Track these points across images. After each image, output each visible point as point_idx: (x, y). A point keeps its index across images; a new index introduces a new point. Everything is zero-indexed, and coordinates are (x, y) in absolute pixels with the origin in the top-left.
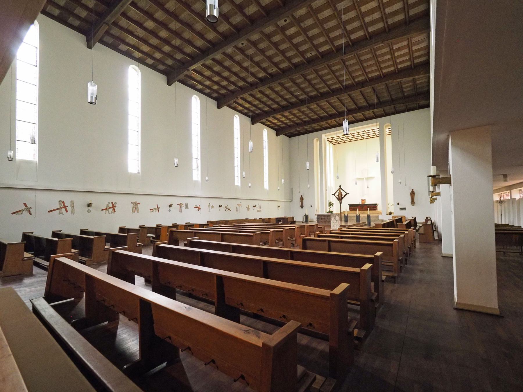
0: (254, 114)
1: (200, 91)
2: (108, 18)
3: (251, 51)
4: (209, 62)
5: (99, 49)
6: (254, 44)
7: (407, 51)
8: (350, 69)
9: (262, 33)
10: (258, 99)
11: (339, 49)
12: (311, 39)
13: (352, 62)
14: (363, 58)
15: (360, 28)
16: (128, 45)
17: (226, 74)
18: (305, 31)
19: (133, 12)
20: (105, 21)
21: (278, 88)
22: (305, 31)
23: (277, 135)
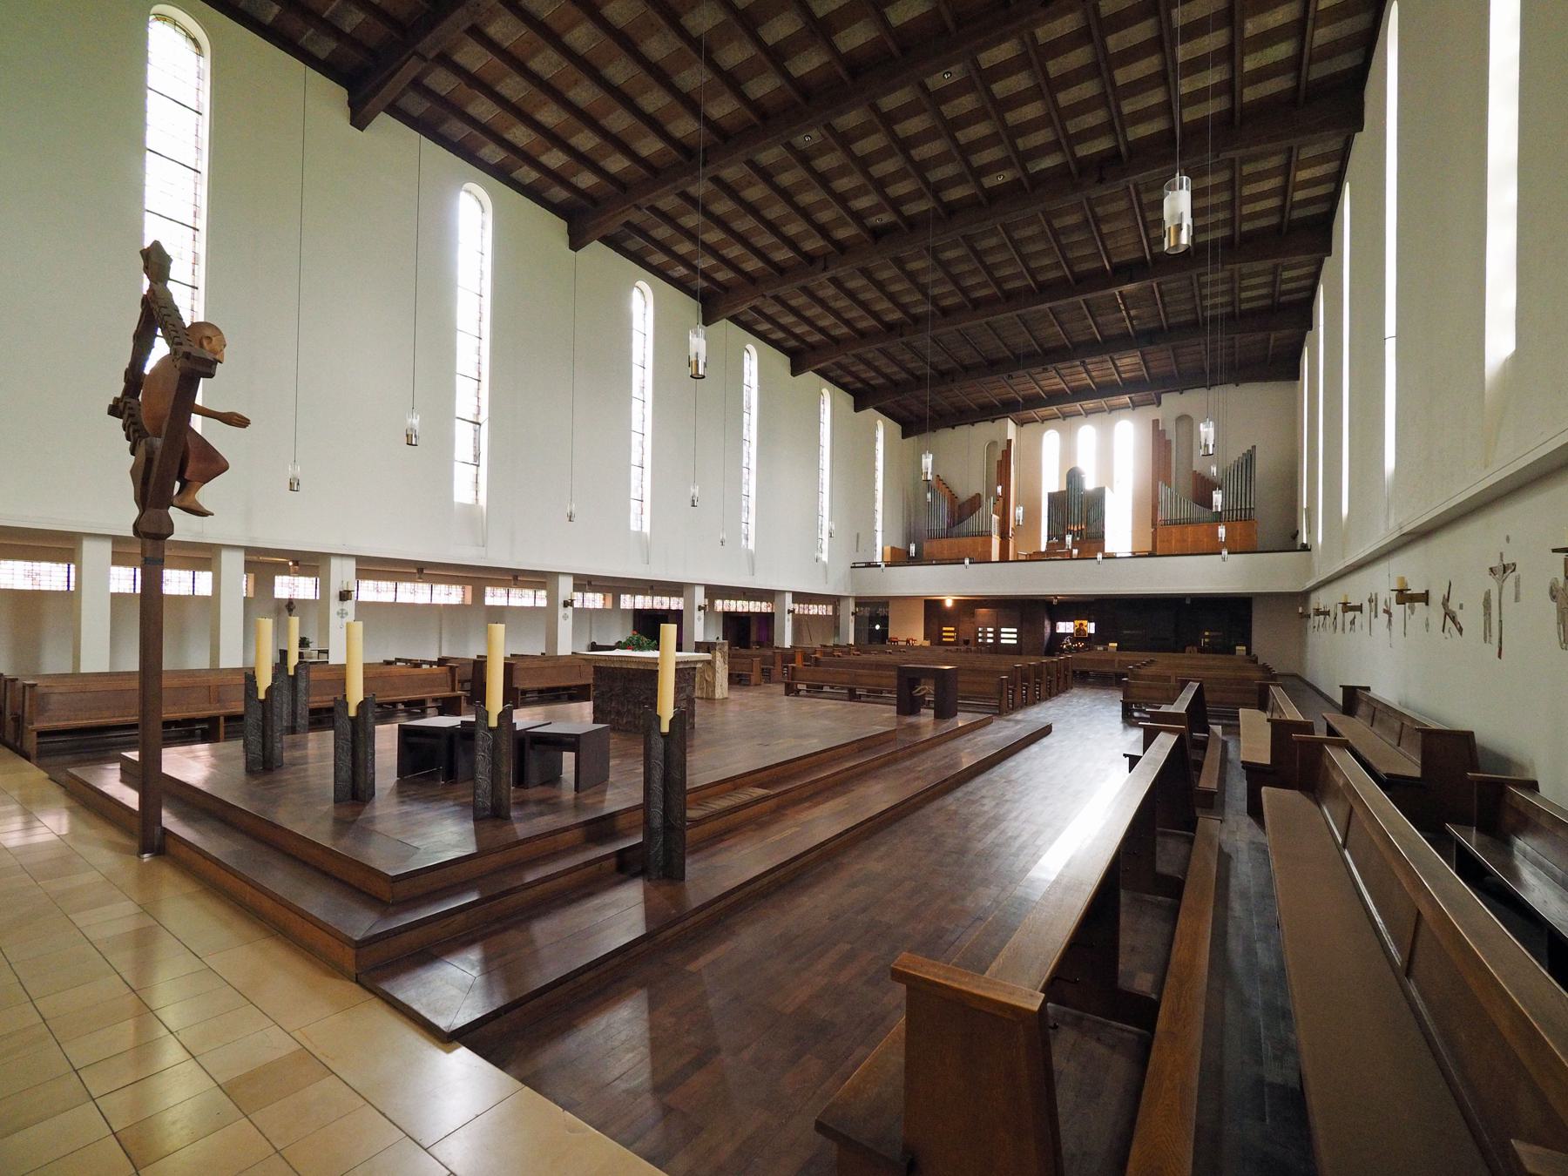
0: (803, 346)
1: (659, 272)
2: (428, 40)
3: (755, 193)
4: (668, 202)
5: (388, 131)
6: (805, 158)
7: (1224, 197)
8: (1105, 229)
9: (829, 127)
10: (795, 311)
11: (994, 195)
12: (921, 168)
13: (993, 242)
14: (1020, 234)
15: (1054, 147)
16: (472, 121)
17: (714, 236)
18: (952, 126)
19: (504, 29)
20: (420, 47)
21: (856, 283)
22: (952, 126)
23: (858, 407)
